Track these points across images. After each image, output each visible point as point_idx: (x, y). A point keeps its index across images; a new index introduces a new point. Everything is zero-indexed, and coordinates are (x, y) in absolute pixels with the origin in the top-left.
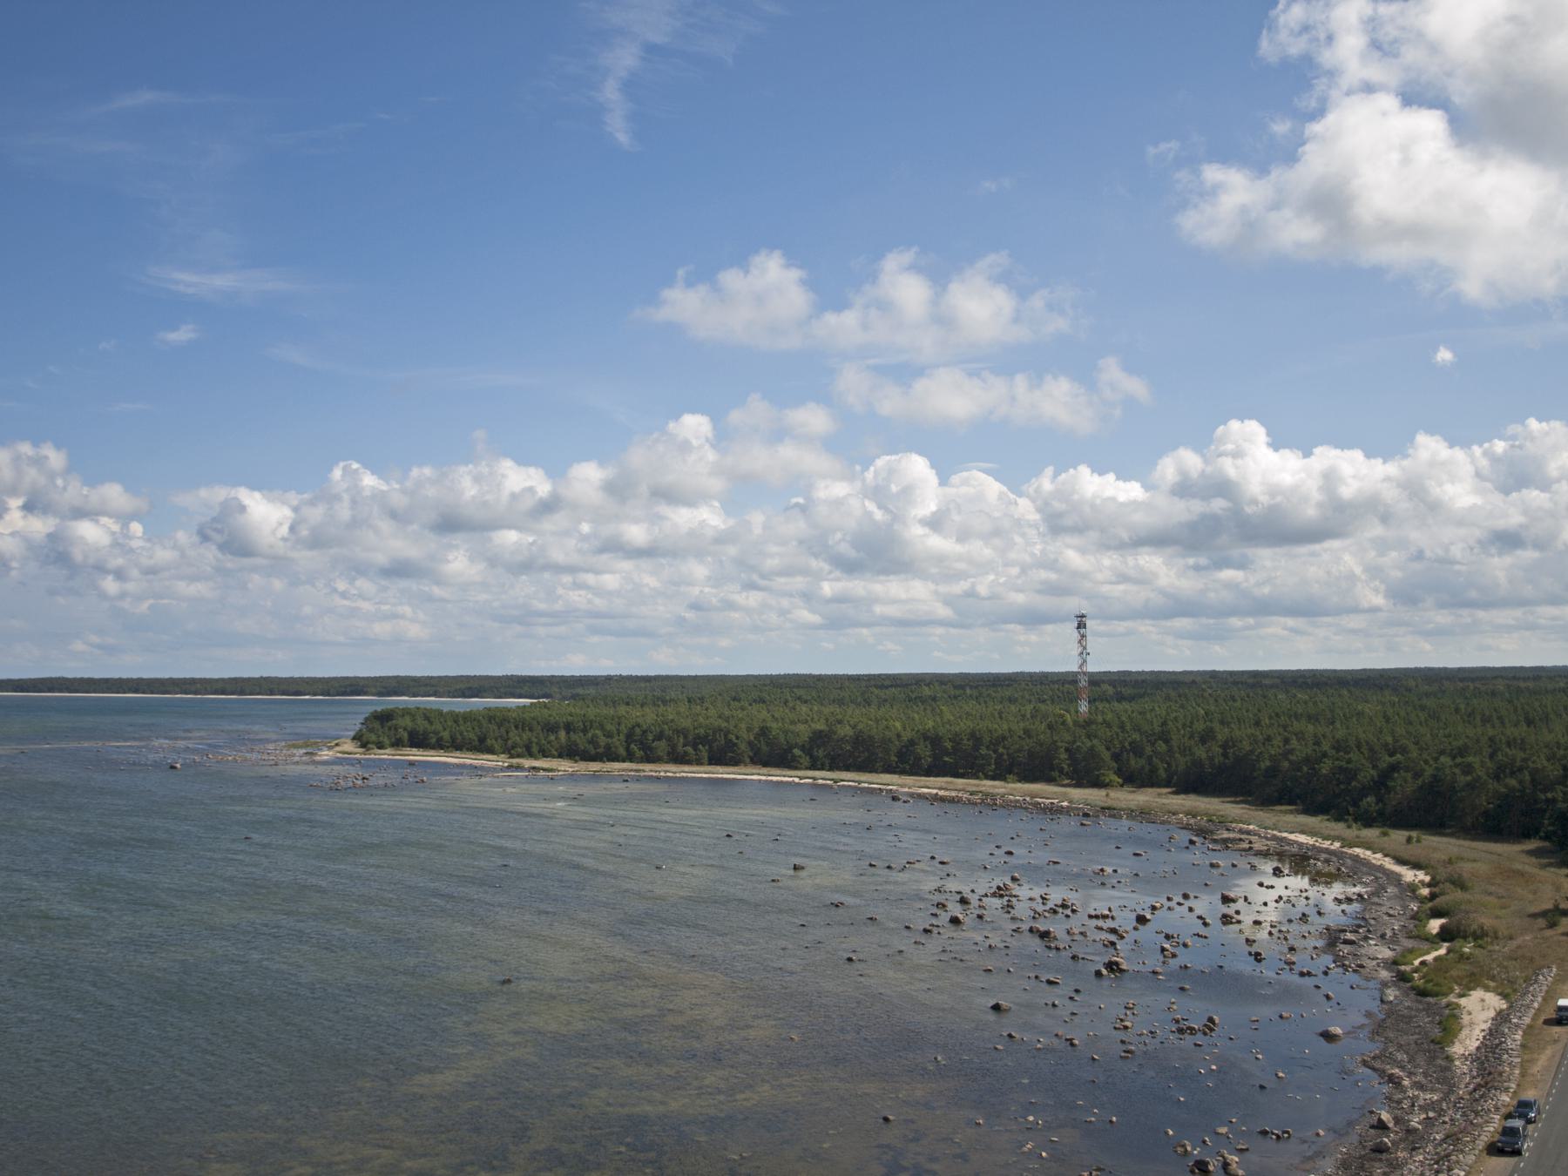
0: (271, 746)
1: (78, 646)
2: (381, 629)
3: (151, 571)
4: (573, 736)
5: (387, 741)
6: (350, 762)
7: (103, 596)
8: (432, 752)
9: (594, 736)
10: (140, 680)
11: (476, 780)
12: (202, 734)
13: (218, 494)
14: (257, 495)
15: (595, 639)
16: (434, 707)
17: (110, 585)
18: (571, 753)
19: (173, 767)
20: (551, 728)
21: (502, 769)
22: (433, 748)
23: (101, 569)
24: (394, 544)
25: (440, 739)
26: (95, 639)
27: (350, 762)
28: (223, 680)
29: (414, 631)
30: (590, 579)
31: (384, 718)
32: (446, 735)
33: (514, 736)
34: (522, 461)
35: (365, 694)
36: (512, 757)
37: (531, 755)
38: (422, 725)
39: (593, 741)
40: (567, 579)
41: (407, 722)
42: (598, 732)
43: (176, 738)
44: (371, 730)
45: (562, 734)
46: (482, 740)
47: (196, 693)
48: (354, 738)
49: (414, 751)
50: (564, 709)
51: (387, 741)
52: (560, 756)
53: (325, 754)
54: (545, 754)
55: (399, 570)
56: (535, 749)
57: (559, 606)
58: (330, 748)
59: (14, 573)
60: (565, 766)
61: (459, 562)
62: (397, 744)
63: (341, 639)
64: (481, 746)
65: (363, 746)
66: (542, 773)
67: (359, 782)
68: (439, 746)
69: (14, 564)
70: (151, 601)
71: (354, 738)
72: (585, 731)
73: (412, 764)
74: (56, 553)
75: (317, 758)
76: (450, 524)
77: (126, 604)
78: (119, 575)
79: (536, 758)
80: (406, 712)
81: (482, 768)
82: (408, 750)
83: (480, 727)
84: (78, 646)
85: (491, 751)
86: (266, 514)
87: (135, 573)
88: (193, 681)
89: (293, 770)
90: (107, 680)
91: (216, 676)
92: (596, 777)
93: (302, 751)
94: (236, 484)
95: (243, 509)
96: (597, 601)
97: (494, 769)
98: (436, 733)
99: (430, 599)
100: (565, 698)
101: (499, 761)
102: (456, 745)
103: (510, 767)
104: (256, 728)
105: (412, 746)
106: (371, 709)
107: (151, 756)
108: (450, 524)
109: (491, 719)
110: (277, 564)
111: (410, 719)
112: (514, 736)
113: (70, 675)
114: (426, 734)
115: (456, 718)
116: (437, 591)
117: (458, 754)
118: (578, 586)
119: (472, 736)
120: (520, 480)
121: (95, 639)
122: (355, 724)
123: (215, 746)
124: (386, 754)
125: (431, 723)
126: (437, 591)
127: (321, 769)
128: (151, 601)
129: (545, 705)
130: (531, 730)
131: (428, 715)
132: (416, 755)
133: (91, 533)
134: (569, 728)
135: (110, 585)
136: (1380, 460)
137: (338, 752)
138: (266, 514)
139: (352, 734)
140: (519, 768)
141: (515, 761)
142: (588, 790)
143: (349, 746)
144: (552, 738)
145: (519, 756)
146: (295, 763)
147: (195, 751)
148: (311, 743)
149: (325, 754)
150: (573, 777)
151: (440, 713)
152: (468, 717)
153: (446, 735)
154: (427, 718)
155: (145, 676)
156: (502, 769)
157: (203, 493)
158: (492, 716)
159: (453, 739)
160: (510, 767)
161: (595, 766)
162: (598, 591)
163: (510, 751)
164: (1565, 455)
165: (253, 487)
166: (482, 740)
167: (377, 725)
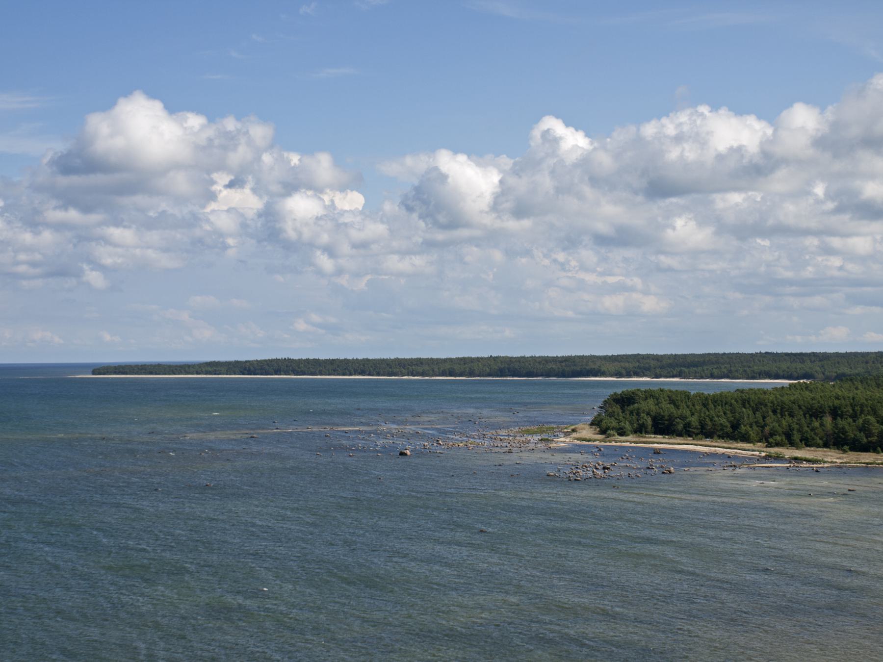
0: (503, 432)
1: (301, 325)
2: (613, 303)
3: (363, 245)
4: (841, 423)
5: (628, 426)
6: (588, 450)
7: (320, 272)
8: (679, 440)
9: (866, 422)
10: (366, 361)
11: (729, 472)
12: (432, 417)
13: (414, 165)
14: (462, 158)
15: (858, 310)
16: (680, 388)
17: (326, 263)
18: (838, 441)
19: (402, 454)
20: (815, 413)
21: (760, 459)
22: (680, 435)
23: (311, 245)
24: (609, 212)
25: (687, 426)
26: (315, 318)
27: (588, 450)
28: (451, 360)
29: (650, 304)
30: (836, 242)
31: (625, 401)
32: (694, 420)
33: (772, 422)
34: (739, 110)
35: (603, 374)
36: (770, 445)
37: (792, 444)
38: (667, 409)
39: (864, 429)
40: (812, 242)
41: (650, 405)
42: (872, 419)
43: (404, 423)
44: (611, 415)
45: (828, 420)
46: (735, 426)
47: (423, 375)
48: (592, 424)
49: (659, 438)
50: (830, 392)
51: (628, 426)
52: (826, 445)
53: (562, 441)
54: (807, 442)
55: (620, 238)
56: (796, 437)
57: (809, 272)
58: (567, 434)
59: (231, 253)
60: (832, 457)
61: (685, 230)
62: (640, 430)
63: (570, 314)
64: (734, 433)
65: (603, 432)
66: (805, 464)
67: (600, 473)
68: (687, 432)
69: (231, 241)
70: (369, 277)
71: (592, 424)
72: (854, 417)
73: (657, 452)
74: (269, 228)
75: (553, 445)
76: (660, 187)
77: (344, 281)
78: (329, 250)
79: (798, 448)
80: (649, 395)
81: (735, 457)
82: (652, 437)
83: (733, 411)
84: (301, 325)
85: (745, 439)
86: (473, 180)
87: (346, 248)
88: (420, 362)
89: (529, 458)
90: (332, 362)
91: (443, 356)
92: (868, 469)
93: (536, 438)
94: (433, 149)
95: (443, 177)
96: (850, 266)
97: (751, 459)
98: (683, 418)
99: (660, 269)
100: (828, 379)
101: (757, 450)
102: (706, 432)
103: (768, 458)
104: (485, 412)
105: (655, 433)
106: (610, 392)
107: (380, 442)
108: (660, 187)
109: (745, 402)
110: (492, 237)
111: (661, 404)
112: (772, 422)
113: (296, 356)
114: (671, 419)
115: (706, 401)
116: (665, 260)
117: (708, 442)
118: (829, 251)
119: (723, 420)
120: (733, 133)
121: (315, 318)
122: (593, 408)
123: (445, 432)
124: (628, 441)
125: (677, 407)
126: (665, 260)
127: (558, 458)
128: (369, 277)
129: (807, 387)
130: (791, 415)
131: (674, 398)
132: (661, 443)
133: (301, 207)
134: (835, 413)
135: (326, 263)
136: (710, 109)
137: (575, 439)
138: (473, 180)
139: (590, 418)
140: (778, 458)
141: (774, 450)
142: (861, 484)
143: (587, 432)
144: (816, 424)
145: (778, 445)
146: (530, 452)
147: (423, 436)
148: (546, 430)
149: (562, 441)
150: (840, 470)
151: (687, 396)
152: (719, 400)
153: (694, 420)
154: (672, 402)
155: (372, 356)
156: (760, 459)
157: (409, 161)
158: (745, 399)
159: (703, 426)
160: (768, 458)
161: (867, 457)
162: (850, 256)
163: (767, 439)
164: (882, 82)
165: (456, 150)
166: (735, 426)
167: (617, 409)
